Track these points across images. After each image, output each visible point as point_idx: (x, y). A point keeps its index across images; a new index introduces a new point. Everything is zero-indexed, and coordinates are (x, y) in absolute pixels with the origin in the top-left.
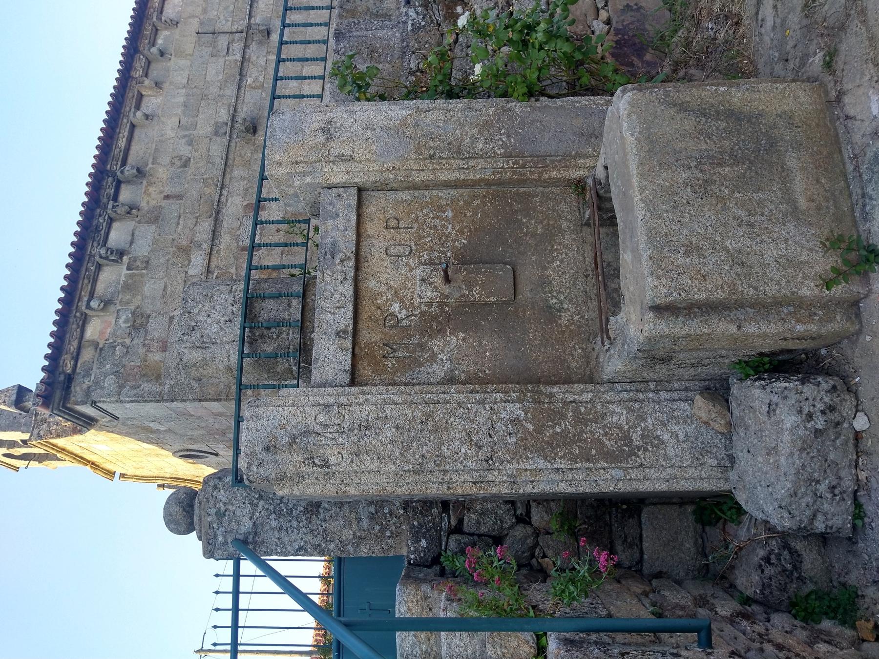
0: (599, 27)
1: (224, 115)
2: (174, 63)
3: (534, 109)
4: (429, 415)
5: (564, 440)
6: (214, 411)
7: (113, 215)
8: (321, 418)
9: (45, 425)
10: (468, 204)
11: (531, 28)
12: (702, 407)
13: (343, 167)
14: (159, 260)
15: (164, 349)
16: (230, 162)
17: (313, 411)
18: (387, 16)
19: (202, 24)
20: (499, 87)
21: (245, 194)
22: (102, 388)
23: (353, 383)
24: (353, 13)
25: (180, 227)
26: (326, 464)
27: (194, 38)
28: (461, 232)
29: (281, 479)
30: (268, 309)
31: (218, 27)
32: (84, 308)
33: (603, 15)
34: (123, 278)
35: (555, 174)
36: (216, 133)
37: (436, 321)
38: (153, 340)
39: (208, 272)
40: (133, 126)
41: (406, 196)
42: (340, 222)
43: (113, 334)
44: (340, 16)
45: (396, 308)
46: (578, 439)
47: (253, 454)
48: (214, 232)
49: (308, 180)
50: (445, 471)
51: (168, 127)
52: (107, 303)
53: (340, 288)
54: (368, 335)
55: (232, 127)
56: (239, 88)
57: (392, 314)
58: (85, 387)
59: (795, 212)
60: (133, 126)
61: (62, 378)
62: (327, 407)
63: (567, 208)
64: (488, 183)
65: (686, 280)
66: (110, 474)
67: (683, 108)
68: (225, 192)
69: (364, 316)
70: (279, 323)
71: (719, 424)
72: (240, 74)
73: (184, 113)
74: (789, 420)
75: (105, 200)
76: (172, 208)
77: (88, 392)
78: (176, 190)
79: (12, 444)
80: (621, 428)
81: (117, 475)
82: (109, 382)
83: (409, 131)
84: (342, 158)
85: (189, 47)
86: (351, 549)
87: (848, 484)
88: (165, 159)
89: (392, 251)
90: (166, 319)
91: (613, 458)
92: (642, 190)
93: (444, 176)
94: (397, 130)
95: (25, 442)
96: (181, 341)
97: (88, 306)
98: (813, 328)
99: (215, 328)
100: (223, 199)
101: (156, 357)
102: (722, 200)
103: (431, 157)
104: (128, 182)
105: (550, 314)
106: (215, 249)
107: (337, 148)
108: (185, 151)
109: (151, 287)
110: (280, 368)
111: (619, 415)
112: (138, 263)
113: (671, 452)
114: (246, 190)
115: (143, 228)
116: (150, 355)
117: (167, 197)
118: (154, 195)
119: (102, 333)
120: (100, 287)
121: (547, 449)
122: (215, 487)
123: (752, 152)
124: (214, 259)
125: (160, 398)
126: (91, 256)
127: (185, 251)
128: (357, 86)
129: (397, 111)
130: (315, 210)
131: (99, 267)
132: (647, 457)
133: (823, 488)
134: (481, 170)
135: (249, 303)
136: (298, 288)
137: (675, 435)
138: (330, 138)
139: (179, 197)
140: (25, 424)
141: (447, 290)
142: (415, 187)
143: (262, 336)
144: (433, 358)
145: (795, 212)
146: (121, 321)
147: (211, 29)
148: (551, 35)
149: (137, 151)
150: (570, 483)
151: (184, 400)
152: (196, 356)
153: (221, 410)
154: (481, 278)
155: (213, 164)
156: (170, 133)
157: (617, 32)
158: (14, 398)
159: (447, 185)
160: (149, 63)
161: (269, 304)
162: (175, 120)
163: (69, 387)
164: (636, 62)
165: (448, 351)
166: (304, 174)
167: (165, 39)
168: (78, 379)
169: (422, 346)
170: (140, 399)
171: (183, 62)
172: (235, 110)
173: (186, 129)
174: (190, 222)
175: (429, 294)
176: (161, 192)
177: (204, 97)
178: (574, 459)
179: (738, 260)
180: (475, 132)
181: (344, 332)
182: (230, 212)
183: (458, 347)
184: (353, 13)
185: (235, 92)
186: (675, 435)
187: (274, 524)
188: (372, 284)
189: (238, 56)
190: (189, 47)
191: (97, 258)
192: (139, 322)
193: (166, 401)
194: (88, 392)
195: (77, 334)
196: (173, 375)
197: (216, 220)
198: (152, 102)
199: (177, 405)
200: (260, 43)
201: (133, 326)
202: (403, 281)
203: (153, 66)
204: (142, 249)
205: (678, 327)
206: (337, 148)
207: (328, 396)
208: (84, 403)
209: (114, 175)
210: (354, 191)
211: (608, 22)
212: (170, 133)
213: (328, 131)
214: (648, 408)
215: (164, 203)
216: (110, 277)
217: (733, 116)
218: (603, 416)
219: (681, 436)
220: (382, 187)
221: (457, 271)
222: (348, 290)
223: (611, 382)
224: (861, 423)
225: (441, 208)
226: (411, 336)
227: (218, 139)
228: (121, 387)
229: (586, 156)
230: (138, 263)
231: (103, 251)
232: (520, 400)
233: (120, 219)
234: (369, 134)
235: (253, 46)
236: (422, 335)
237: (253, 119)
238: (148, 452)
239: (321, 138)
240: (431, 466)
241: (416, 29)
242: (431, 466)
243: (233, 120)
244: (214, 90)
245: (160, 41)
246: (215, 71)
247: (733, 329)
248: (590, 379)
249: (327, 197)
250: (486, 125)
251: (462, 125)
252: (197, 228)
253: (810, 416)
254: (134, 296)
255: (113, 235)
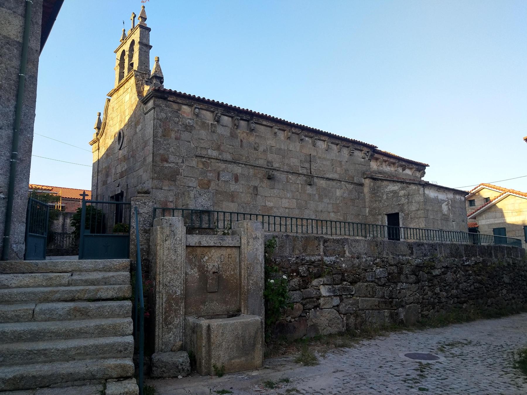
0: (289, 319)
1: (276, 165)
2: (298, 145)
3: (261, 297)
4: (178, 268)
5: (170, 306)
6: (147, 158)
7: (234, 118)
8: (178, 239)
9: (141, 78)
10: (235, 278)
11: (283, 296)
12: (179, 343)
13: (246, 242)
14: (215, 137)
15: (177, 139)
16: (256, 168)
17: (180, 236)
18: (293, 251)
19: (314, 156)
20: (267, 286)
21: (242, 174)
22: (161, 112)
23: (187, 246)
24: (294, 240)
25: (228, 146)
26: (166, 240)
27: (308, 153)
28: (227, 276)
29: (162, 228)
30: (205, 218)
31: (313, 163)
32: (195, 106)
33: (293, 320)
34: (207, 122)
35: (243, 303)
36: (268, 162)
37: (202, 269)
38: (181, 134)
39: (209, 158)
40: (272, 127)
41: (238, 260)
42: (231, 242)
43: (183, 117)
44: (293, 236)
45: (206, 258)
46: (170, 310)
47: (169, 220)
48: (226, 161)
49: (243, 233)
50: (163, 273)
51: (271, 142)
52: (197, 115)
53: (212, 242)
54: (199, 250)
55: (271, 169)
56: (287, 172)
57: (205, 257)
58: (161, 105)
59: (231, 359)
60: (272, 127)
61: (166, 96)
62: (181, 240)
63: (233, 308)
64: (240, 284)
65: (216, 332)
66: (111, 95)
67: (256, 333)
68: (243, 166)
69: (204, 249)
70: (201, 221)
71: (174, 348)
72: (293, 173)
73: (277, 148)
74: (181, 360)
75: (241, 116)
76: (237, 143)
77: (159, 106)
78: (244, 145)
79: (131, 57)
80: (173, 322)
81: (109, 98)
82: (163, 115)
83: (255, 261)
84: (248, 242)
85: (304, 151)
86: (133, 242)
87: (165, 375)
88: (257, 140)
89: (222, 256)
90: (189, 140)
91: (165, 320)
92: (237, 322)
93: (243, 271)
94: (256, 258)
95: (132, 65)
96: (197, 191)
97: (196, 108)
98: (203, 364)
99: (200, 201)
100: (240, 165)
101: (173, 135)
102: (234, 341)
103: (248, 268)
104: (248, 125)
105: (203, 302)
106: (219, 161)
107: (251, 241)
108: (261, 149)
109: (203, 133)
110: (187, 220)
111: (176, 321)
112: (214, 128)
113: (166, 336)
114: (244, 175)
115: (229, 131)
116: (174, 132)
117: (241, 141)
118: (242, 135)
119: (184, 112)
120: (204, 112)
121: (168, 301)
122: (153, 202)
123: (246, 348)
124: (215, 161)
125: (155, 136)
126: (217, 109)
127: (218, 148)
128: (269, 246)
129: (261, 258)
130: (233, 233)
131: (213, 112)
132: (165, 329)
133: (164, 369)
134: (244, 282)
135: (208, 212)
136: (211, 226)
137: (171, 337)
138: (254, 239)
139: (241, 146)
140: (141, 68)
141: (211, 272)
142: (240, 263)
143: (197, 215)
144: (192, 269)
145: (231, 359)
146: (189, 120)
147: (312, 160)
148: (281, 302)
149: (261, 129)
150: (159, 308)
151: (153, 146)
152: (192, 195)
153: (148, 161)
154: (214, 282)
155: (255, 161)
156: (268, 142)
157: (287, 324)
158: (158, 75)
159: (240, 272)
160: (298, 134)
161: (207, 218)
162: (274, 145)
163: (161, 98)
164: (278, 330)
165: (194, 273)
166: (244, 232)
167: (308, 141)
168: (165, 102)
169: (195, 265)
170: (155, 128)
171: (298, 148)
172: (278, 170)
173: (270, 149)
174: (230, 151)
175: (210, 267)
176: (244, 139)
177: (284, 157)
178: (165, 309)
179: (220, 345)
180: (255, 280)
181: (200, 244)
182: (235, 167)
183: (195, 276)
184: (294, 240)
185: (285, 170)
186: (171, 337)
187: (141, 219)
188: (213, 251)
189: (301, 172)
190: (304, 151)
191: (216, 112)
192: (188, 128)
193: (153, 139)
194: (159, 106)
195: (184, 102)
196: (165, 142)
197: (232, 162)
198: (282, 135)
199: (151, 143)
200: (306, 181)
201: (187, 125)
202: (213, 260)
203: (297, 136)
204: (220, 130)
205: (204, 332)
206: (251, 241)
207: (184, 240)
208: (154, 104)
209: (252, 119)
210: (239, 245)
211: (290, 322)
212: (268, 142)
213: (256, 238)
214: (178, 329)
215: (239, 140)
216: (208, 116)
217: (254, 345)
218: (176, 317)
219: (171, 339)
220: (240, 253)
221: (216, 276)
222: (212, 244)
223: (185, 319)
224: (180, 377)
225: (234, 270)
226: (198, 262)
227: (266, 163)
228: (160, 120)
229: (247, 312)
230: (214, 128)
231: (219, 114)
232: (181, 293)
233: (233, 121)
234: (255, 250)
235: (305, 178)
236: (198, 266)
237: (274, 178)
238: (123, 118)
239: (254, 236)
240: (165, 269)
241: (289, 260)
242: (165, 269)
243: (274, 169)
244: (286, 161)
245: (307, 139)
246: (294, 162)
247: (204, 345)
248: (186, 314)
249: (238, 238)
250: (257, 284)
251: (257, 277)
252: (228, 154)
253: (182, 365)
254: (199, 126)
255: (226, 118)
